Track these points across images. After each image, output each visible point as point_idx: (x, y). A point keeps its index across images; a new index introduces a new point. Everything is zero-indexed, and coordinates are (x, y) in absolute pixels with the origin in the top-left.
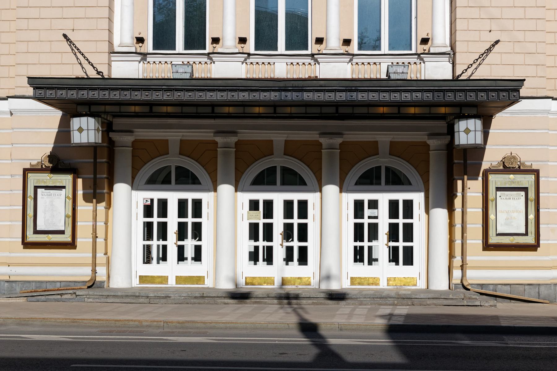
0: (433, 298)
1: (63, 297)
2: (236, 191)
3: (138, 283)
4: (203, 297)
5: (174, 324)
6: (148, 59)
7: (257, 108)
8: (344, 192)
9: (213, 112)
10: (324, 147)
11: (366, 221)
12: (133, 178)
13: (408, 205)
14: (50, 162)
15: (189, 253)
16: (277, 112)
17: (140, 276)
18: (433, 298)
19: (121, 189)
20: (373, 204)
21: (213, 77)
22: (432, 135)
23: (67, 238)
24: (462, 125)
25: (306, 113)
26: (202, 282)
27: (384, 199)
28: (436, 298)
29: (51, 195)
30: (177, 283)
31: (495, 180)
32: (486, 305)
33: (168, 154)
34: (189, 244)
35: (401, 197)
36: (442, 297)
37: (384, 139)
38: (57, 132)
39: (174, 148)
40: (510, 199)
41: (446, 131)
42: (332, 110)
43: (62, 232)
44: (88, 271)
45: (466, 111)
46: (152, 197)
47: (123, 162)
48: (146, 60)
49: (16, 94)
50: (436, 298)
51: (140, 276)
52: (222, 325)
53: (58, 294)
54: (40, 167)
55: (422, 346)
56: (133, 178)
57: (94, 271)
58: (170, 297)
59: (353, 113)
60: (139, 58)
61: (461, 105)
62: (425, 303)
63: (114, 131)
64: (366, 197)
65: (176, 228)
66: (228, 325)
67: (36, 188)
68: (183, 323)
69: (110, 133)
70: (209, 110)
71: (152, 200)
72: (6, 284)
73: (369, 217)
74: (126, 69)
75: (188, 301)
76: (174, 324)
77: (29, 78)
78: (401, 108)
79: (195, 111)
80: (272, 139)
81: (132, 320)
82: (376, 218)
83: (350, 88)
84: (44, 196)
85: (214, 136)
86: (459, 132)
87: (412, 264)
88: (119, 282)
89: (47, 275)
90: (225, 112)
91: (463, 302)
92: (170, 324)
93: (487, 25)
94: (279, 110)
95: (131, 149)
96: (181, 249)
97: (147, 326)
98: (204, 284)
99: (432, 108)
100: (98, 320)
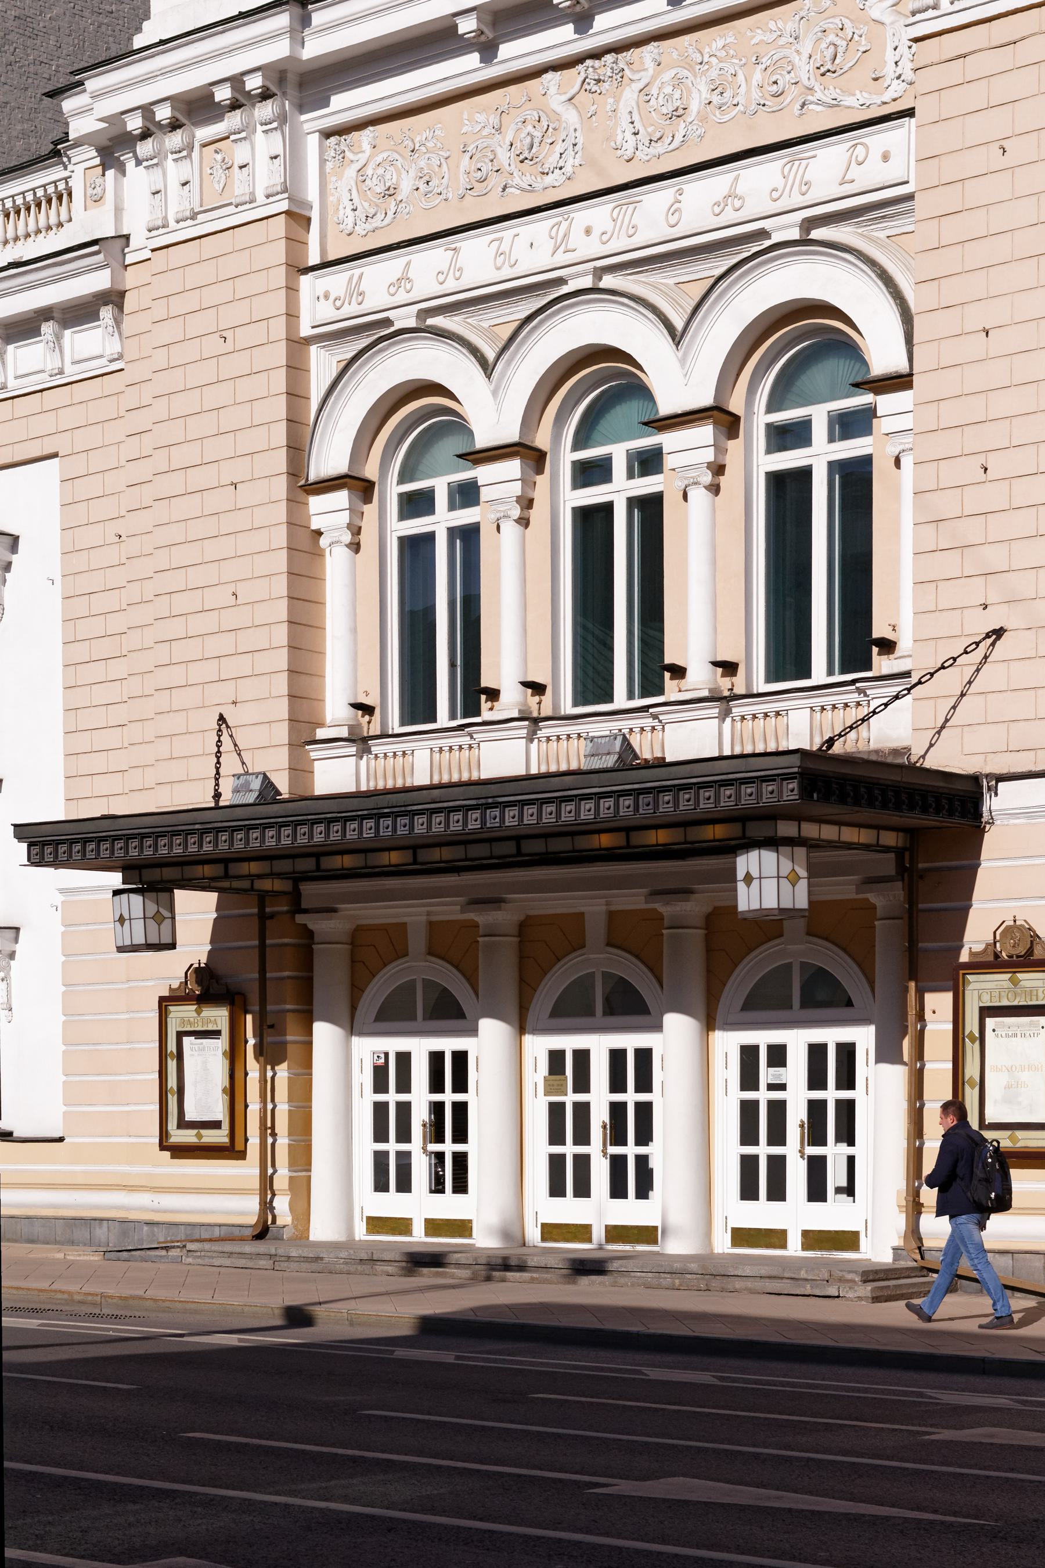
0: (770, 1277)
1: (170, 1253)
2: (522, 1030)
3: (730, 1245)
4: (372, 1261)
5: (114, 1301)
6: (737, 711)
7: (246, 864)
8: (719, 1029)
9: (318, 868)
10: (879, 913)
11: (763, 1096)
12: (353, 1008)
13: (847, 1053)
14: (199, 982)
15: (835, 1177)
16: (420, 859)
17: (733, 1229)
18: (770, 1277)
19: (325, 1035)
20: (778, 1055)
21: (485, 775)
22: (872, 881)
23: (219, 1137)
24: (747, 862)
25: (366, 867)
26: (467, 1233)
27: (797, 1041)
28: (775, 1277)
29: (203, 1049)
30: (544, 1239)
31: (983, 988)
32: (850, 1295)
33: (781, 935)
34: (834, 1152)
35: (831, 1036)
36: (786, 1275)
37: (593, 907)
38: (215, 920)
39: (417, 942)
40: (1016, 1035)
41: (893, 872)
42: (509, 848)
43: (216, 1125)
44: (253, 1204)
45: (756, 830)
46: (385, 1049)
47: (331, 973)
48: (370, 752)
49: (1012, 771)
50: (775, 1277)
51: (733, 1229)
52: (179, 1306)
53: (162, 1248)
54: (991, 958)
55: (624, 1379)
56: (353, 1008)
57: (267, 1206)
58: (322, 1259)
59: (547, 853)
60: (353, 750)
61: (741, 818)
62: (730, 1287)
63: (306, 911)
64: (763, 1038)
65: (803, 1115)
66: (188, 1306)
67: (180, 1035)
68: (126, 1298)
69: (297, 916)
70: (509, 848)
71: (387, 1055)
72: (146, 1228)
73: (771, 1087)
74: (335, 775)
75: (352, 1268)
76: (114, 1301)
77: (15, 826)
78: (633, 835)
79: (569, 847)
80: (583, 909)
81: (60, 1291)
82: (782, 1087)
83: (483, 801)
84: (194, 1053)
85: (463, 911)
86: (145, 918)
87: (409, 1191)
88: (324, 1227)
89: (204, 1212)
90: (706, 838)
91: (805, 1287)
92: (110, 1300)
93: (975, 591)
94: (424, 855)
95: (517, 939)
96: (817, 1168)
97: (79, 1302)
98: (411, 1235)
99: (689, 829)
100: (18, 1288)
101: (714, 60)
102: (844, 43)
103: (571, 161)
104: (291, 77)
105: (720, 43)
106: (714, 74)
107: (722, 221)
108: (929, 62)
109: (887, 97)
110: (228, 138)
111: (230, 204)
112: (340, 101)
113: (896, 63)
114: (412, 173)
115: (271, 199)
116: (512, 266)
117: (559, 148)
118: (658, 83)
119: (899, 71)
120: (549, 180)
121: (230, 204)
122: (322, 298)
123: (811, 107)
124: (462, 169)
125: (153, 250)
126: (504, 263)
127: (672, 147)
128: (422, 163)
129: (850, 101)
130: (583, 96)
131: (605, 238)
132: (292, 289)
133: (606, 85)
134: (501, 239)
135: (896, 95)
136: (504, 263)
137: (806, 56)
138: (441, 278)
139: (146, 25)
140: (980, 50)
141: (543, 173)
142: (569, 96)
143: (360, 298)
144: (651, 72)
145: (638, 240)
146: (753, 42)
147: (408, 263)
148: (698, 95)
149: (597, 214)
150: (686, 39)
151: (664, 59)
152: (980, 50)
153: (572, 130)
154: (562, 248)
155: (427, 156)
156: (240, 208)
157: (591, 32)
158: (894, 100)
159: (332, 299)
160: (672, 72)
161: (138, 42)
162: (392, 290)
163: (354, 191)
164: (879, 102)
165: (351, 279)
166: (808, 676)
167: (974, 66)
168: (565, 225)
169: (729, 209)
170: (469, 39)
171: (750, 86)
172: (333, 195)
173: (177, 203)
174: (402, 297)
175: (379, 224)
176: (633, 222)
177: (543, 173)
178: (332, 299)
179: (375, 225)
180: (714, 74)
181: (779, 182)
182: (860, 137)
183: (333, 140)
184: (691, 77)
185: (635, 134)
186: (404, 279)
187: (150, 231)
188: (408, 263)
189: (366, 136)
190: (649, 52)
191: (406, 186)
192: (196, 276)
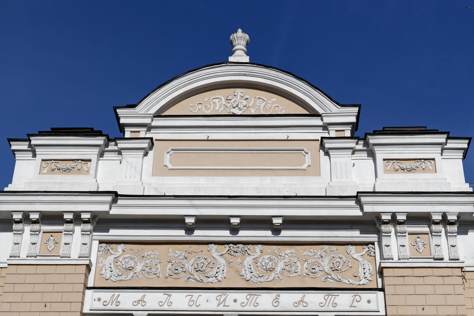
101: (287, 256)
102: (207, 264)
103: (220, 276)
104: (97, 219)
105: (290, 251)
106: (287, 260)
107: (295, 309)
108: (389, 275)
109: (361, 283)
110: (62, 232)
111: (60, 256)
112: (113, 232)
113: (217, 272)
114: (142, 264)
115: (80, 259)
116: (197, 306)
117: (215, 270)
118: (262, 258)
119: (217, 275)
120: (210, 280)
121: (60, 256)
122: (96, 300)
123: (329, 280)
124: (168, 268)
125: (8, 265)
126: (193, 304)
127: (268, 280)
128: (148, 262)
129: (346, 281)
130: (227, 255)
131: (243, 305)
132: (84, 294)
133: (238, 254)
134: (192, 296)
135: (364, 283)
136: (193, 304)
137: (191, 264)
138: (161, 304)
139: (10, 185)
140: (410, 276)
141: (207, 277)
142: (221, 254)
143: (117, 304)
144: (259, 254)
145: (258, 308)
146: (303, 254)
147: (145, 295)
148: (280, 266)
149: (242, 296)
150: (274, 247)
151: (264, 251)
152: (410, 276)
153: (222, 265)
154: (223, 304)
155: (151, 260)
156: (63, 258)
157: (237, 235)
158: (363, 285)
159: (102, 301)
160: (268, 256)
161: (6, 189)
162: (135, 304)
163: (112, 266)
164: (358, 284)
165: (113, 295)
167: (428, 280)
168: (223, 297)
169: (301, 305)
170: (276, 225)
171: (302, 268)
172: (100, 264)
173: (36, 250)
174: (139, 307)
175: (124, 279)
176: (256, 302)
177: (207, 277)
178: (102, 301)
179: (122, 279)
180: (287, 260)
181: (163, 300)
182: (168, 292)
183: (104, 245)
184: (277, 259)
185: (111, 271)
186: (141, 301)
187: (10, 257)
188: (145, 295)
189: (120, 248)
190: (258, 248)
191: (139, 268)
192: (29, 279)
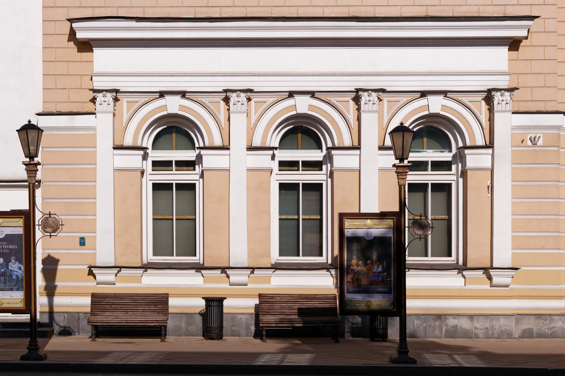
166: (391, 237)
